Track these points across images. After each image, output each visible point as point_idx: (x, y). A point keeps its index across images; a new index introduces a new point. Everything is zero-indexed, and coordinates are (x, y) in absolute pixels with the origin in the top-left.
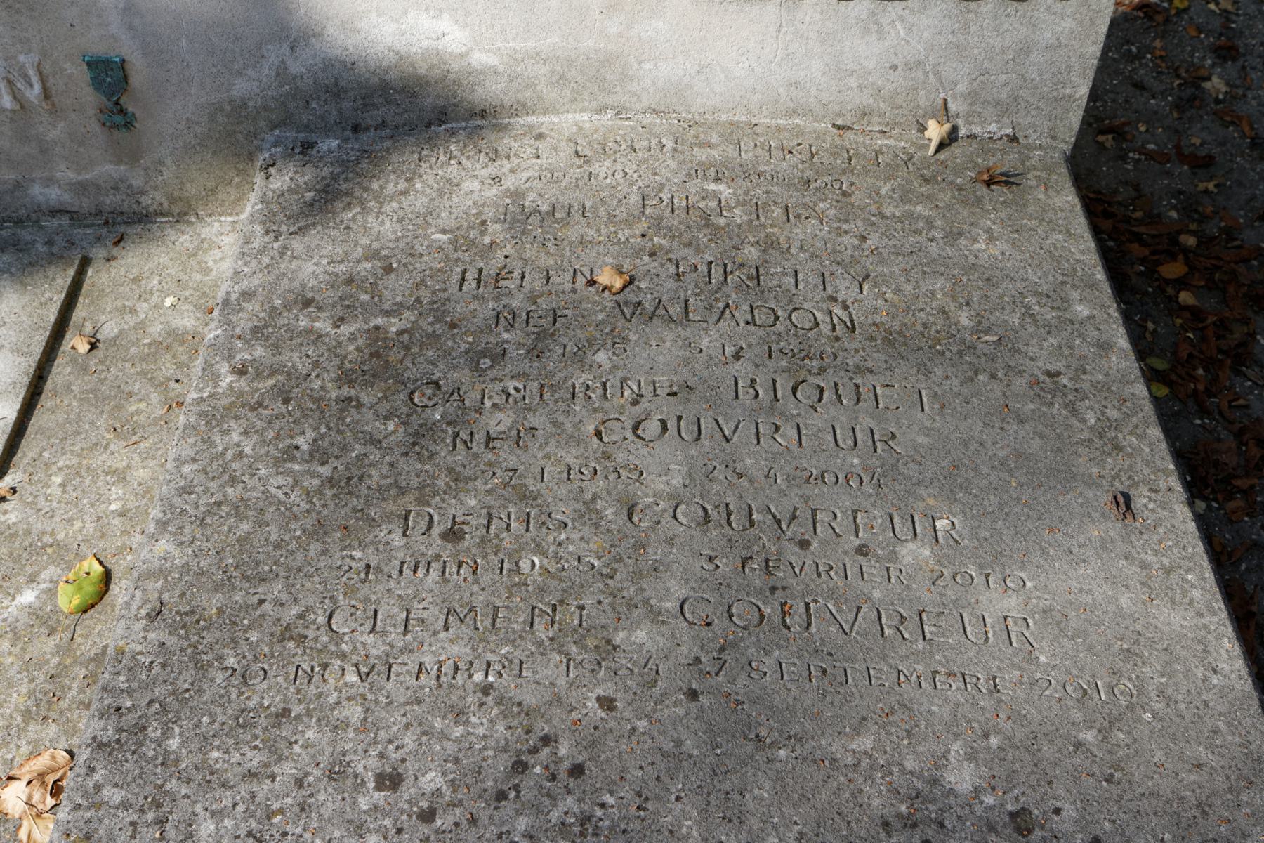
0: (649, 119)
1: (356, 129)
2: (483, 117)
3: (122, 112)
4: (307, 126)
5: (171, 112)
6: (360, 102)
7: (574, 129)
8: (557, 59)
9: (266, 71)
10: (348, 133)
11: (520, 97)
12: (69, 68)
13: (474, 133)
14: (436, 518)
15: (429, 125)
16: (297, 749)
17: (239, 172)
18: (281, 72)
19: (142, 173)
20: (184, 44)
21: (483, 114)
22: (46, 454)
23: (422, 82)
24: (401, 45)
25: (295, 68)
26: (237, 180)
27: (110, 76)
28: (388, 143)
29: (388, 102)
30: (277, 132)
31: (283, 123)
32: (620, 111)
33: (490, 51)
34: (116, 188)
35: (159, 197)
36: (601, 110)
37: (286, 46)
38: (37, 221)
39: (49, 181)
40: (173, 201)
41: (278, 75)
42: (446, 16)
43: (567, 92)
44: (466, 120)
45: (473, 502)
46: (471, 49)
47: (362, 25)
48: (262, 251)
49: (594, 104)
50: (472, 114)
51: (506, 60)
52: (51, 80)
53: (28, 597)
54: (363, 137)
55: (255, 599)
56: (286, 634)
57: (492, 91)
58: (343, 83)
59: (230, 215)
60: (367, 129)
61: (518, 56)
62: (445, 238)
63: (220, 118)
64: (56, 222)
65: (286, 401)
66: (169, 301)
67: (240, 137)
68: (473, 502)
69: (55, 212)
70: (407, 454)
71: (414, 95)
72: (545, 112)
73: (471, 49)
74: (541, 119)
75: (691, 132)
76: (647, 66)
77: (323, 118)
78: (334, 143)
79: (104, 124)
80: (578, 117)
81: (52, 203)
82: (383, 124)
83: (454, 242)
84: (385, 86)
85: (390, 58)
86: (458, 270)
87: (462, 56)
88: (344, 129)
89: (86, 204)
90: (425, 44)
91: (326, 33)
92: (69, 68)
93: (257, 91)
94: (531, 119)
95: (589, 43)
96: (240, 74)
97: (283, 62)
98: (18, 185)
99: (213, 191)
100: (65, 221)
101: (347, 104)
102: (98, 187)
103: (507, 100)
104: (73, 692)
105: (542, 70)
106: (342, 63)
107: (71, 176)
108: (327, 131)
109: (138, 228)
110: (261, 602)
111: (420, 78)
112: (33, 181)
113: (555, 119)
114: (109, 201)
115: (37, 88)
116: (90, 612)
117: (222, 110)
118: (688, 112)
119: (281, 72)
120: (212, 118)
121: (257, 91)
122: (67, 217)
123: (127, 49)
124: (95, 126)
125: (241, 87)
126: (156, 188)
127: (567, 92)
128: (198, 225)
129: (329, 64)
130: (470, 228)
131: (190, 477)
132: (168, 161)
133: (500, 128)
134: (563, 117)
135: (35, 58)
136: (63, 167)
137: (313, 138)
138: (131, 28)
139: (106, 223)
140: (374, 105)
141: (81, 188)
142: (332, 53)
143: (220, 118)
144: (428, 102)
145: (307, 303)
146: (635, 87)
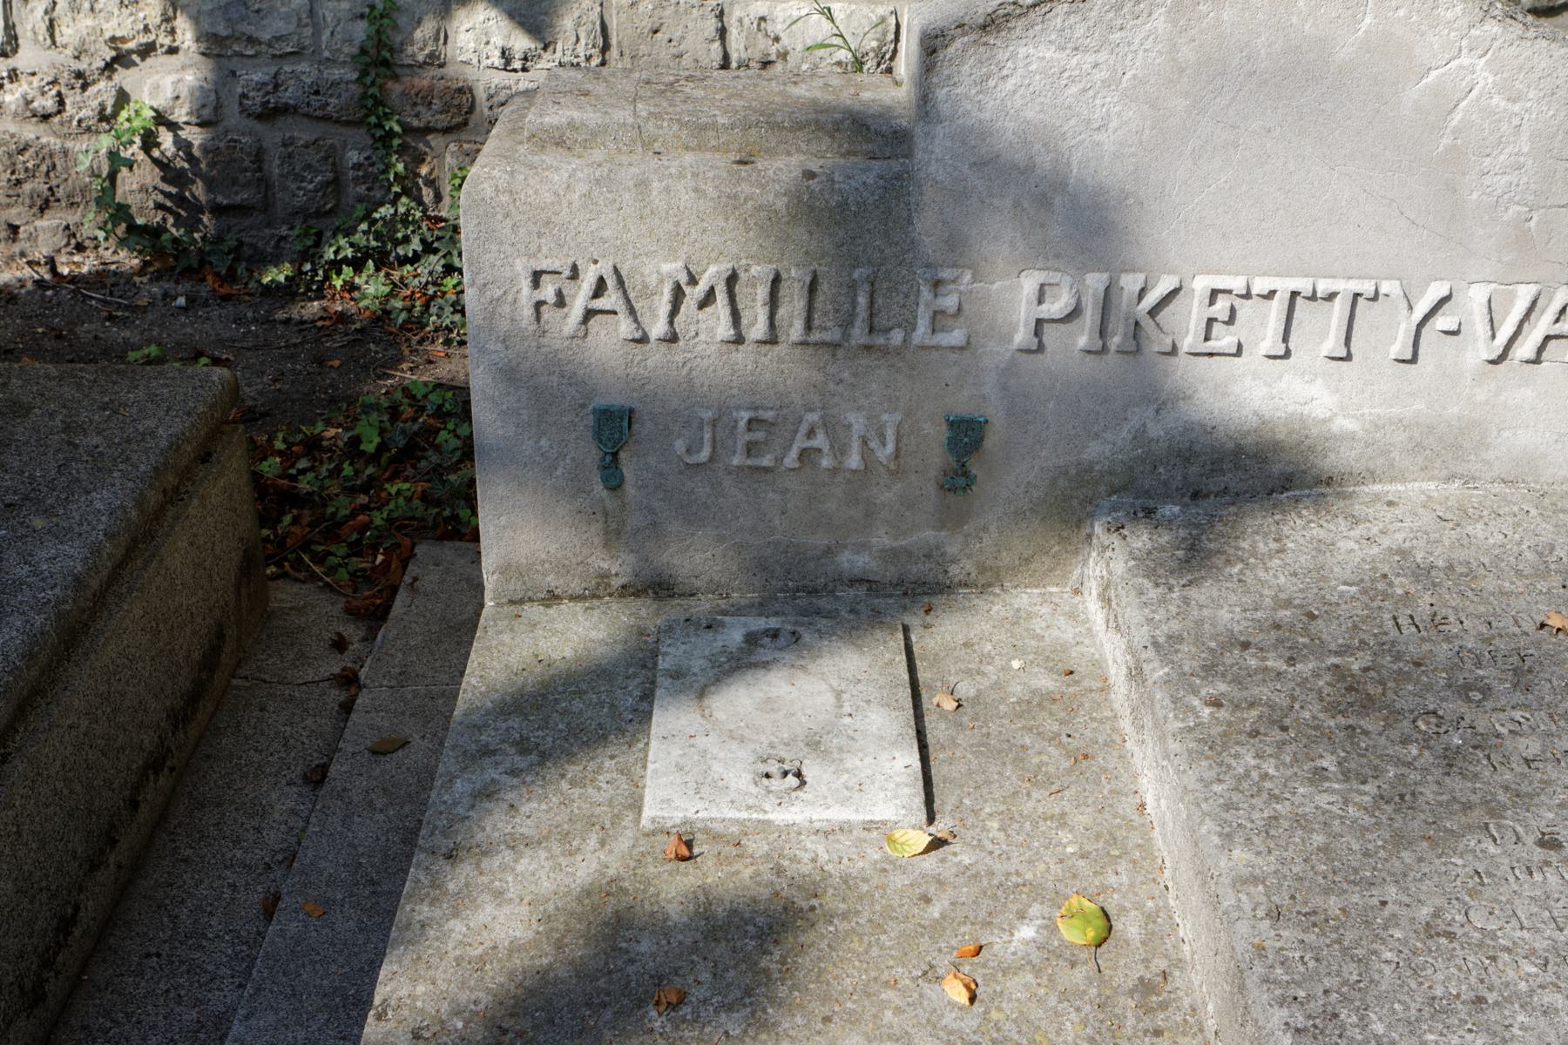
0: (1497, 488)
1: (1196, 495)
2: (1328, 484)
3: (966, 474)
4: (1147, 492)
5: (1014, 472)
6: (1208, 467)
7: (1423, 498)
8: (1418, 424)
9: (1125, 433)
10: (1186, 499)
11: (1371, 465)
12: (928, 428)
13: (1319, 502)
14: (1520, 829)
15: (1270, 494)
16: (1516, 1031)
17: (1063, 540)
18: (1139, 435)
19: (961, 539)
20: (1051, 405)
21: (1329, 481)
22: (967, 801)
23: (1277, 447)
24: (1267, 410)
25: (1155, 430)
26: (1056, 548)
27: (966, 435)
28: (1232, 509)
29: (1237, 467)
30: (1114, 498)
31: (1123, 489)
32: (1469, 480)
33: (1354, 416)
34: (928, 556)
35: (969, 565)
36: (1450, 478)
37: (1152, 408)
38: (832, 592)
39: (862, 547)
40: (982, 569)
41: (1135, 438)
42: (1319, 381)
43: (1420, 460)
44: (1310, 488)
45: (1551, 816)
46: (1336, 415)
47: (1236, 389)
48: (1163, 601)
49: (1445, 472)
50: (1318, 482)
51: (1367, 426)
52: (905, 440)
53: (1027, 932)
54: (1204, 503)
55: (1375, 901)
56: (1430, 931)
57: (1340, 459)
58: (1197, 448)
59: (1036, 587)
60: (1207, 496)
61: (1381, 423)
62: (1354, 589)
63: (1062, 483)
64: (852, 592)
65: (1284, 729)
66: (1016, 664)
67: (1075, 502)
68: (1551, 816)
69: (855, 581)
70: (1448, 774)
71: (1265, 460)
72: (1393, 480)
73: (1336, 415)
74: (1387, 487)
75: (860, 647)
76: (1506, 434)
77: (1165, 483)
78: (1176, 509)
79: (942, 487)
80: (1424, 486)
81: (856, 571)
82: (1225, 491)
83: (1364, 592)
84: (1239, 451)
85: (1254, 421)
86: (1387, 616)
87: (1324, 421)
88: (1183, 495)
89: (891, 573)
90: (1290, 409)
91: (1197, 396)
92: (928, 428)
93: (1108, 453)
94: (1377, 488)
95: (1454, 410)
96: (1097, 436)
97: (1144, 425)
98: (828, 551)
99: (1028, 561)
100: (861, 591)
101: (1194, 469)
102: (910, 554)
103: (1358, 467)
104: (1131, 1021)
105: (1400, 437)
106: (1203, 426)
107: (887, 542)
108: (1167, 497)
109: (943, 599)
110: (1384, 903)
111: (1277, 443)
112: (845, 547)
113: (1400, 487)
114: (916, 569)
115: (890, 448)
116: (1105, 946)
117: (1066, 473)
118: (1536, 482)
119: (1139, 435)
120: (1053, 483)
121: (1108, 453)
122: (865, 587)
123: (994, 412)
124: (931, 489)
125: (1094, 450)
126: (969, 557)
127: (1420, 460)
128: (1006, 597)
129: (1188, 428)
130: (1373, 581)
131: (1227, 795)
132: (993, 528)
133: (1343, 496)
134: (1410, 486)
135: (898, 417)
136: (882, 532)
137: (1151, 503)
138: (1004, 388)
139: (905, 594)
140: (1222, 470)
141: (893, 555)
142: (1196, 416)
143: (1062, 483)
144: (1276, 468)
145: (1245, 645)
146: (1490, 455)
